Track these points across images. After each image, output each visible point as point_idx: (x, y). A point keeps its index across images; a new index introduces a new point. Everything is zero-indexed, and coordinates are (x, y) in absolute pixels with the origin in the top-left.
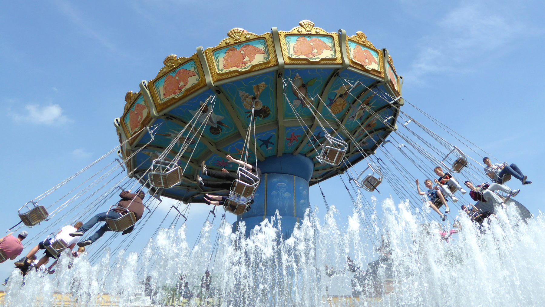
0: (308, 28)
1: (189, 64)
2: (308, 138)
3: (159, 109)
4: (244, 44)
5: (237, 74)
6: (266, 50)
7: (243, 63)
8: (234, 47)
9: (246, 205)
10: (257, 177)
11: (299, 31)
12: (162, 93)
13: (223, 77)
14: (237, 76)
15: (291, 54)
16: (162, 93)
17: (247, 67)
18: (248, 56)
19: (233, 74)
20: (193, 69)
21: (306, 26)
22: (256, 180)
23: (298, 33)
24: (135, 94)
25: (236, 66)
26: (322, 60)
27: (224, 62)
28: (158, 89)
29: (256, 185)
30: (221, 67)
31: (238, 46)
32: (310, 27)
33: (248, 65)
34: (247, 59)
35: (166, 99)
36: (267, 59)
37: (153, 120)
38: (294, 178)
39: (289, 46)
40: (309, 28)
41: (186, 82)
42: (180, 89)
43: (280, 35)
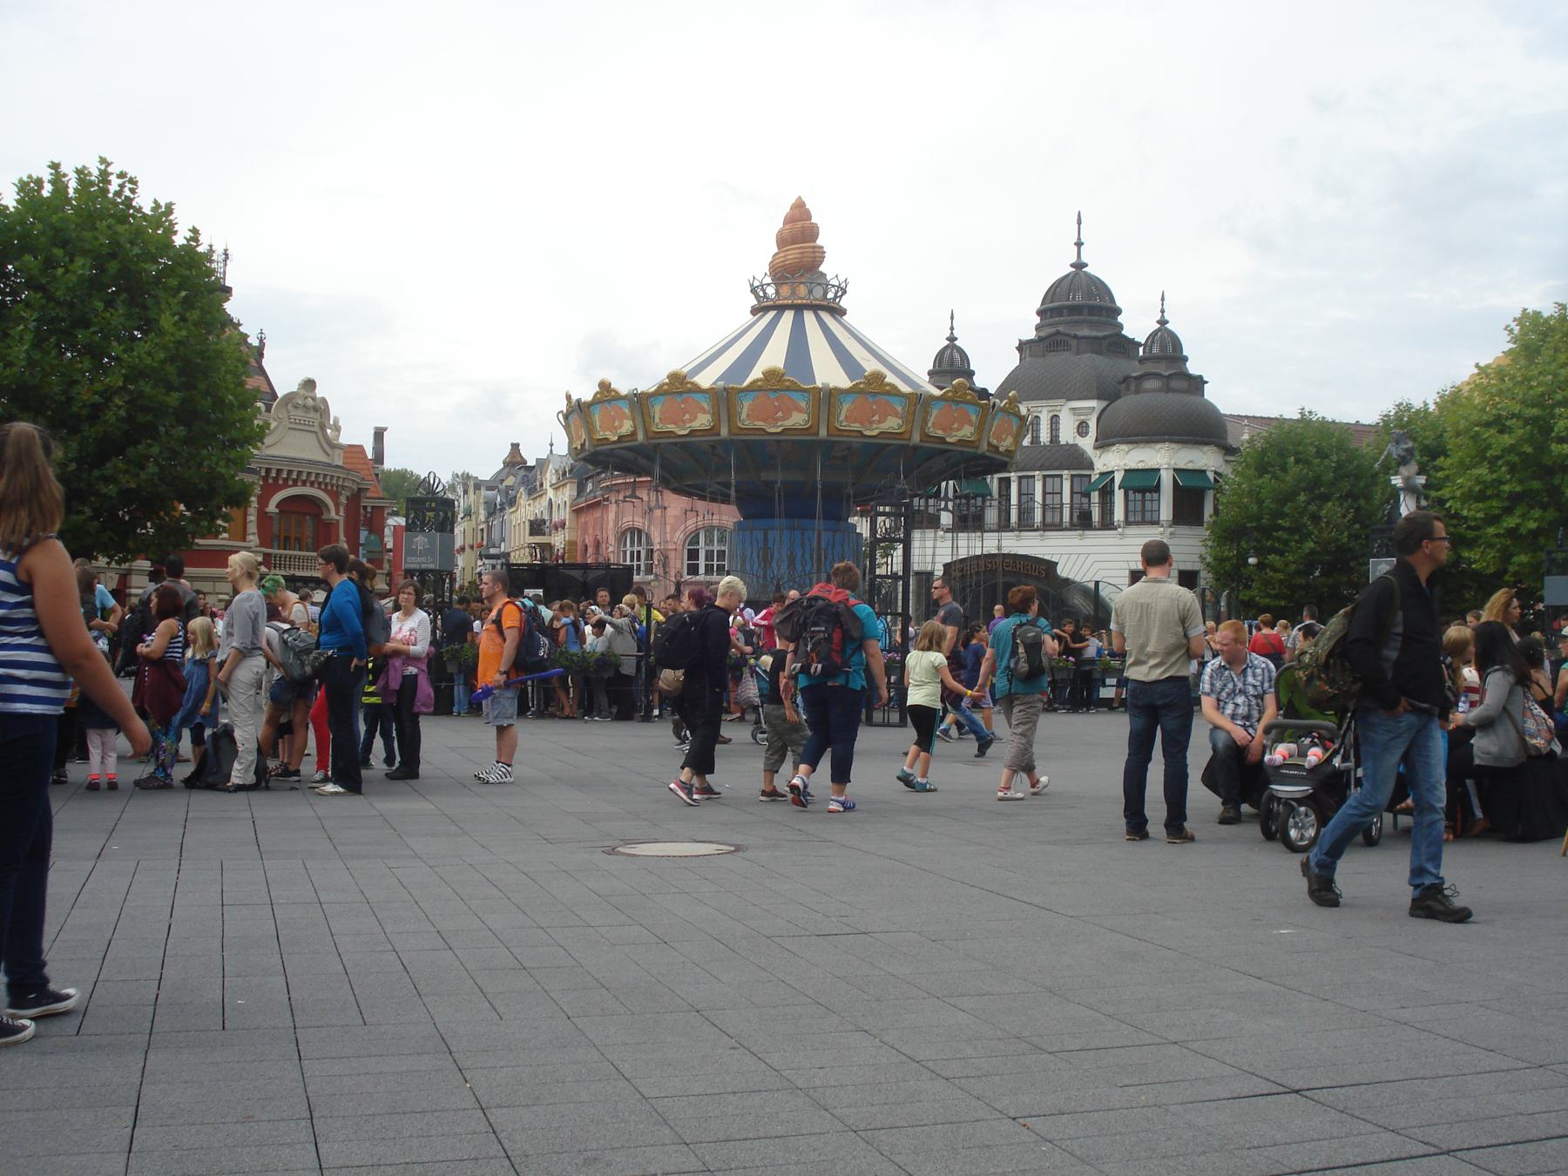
42: (684, 422)
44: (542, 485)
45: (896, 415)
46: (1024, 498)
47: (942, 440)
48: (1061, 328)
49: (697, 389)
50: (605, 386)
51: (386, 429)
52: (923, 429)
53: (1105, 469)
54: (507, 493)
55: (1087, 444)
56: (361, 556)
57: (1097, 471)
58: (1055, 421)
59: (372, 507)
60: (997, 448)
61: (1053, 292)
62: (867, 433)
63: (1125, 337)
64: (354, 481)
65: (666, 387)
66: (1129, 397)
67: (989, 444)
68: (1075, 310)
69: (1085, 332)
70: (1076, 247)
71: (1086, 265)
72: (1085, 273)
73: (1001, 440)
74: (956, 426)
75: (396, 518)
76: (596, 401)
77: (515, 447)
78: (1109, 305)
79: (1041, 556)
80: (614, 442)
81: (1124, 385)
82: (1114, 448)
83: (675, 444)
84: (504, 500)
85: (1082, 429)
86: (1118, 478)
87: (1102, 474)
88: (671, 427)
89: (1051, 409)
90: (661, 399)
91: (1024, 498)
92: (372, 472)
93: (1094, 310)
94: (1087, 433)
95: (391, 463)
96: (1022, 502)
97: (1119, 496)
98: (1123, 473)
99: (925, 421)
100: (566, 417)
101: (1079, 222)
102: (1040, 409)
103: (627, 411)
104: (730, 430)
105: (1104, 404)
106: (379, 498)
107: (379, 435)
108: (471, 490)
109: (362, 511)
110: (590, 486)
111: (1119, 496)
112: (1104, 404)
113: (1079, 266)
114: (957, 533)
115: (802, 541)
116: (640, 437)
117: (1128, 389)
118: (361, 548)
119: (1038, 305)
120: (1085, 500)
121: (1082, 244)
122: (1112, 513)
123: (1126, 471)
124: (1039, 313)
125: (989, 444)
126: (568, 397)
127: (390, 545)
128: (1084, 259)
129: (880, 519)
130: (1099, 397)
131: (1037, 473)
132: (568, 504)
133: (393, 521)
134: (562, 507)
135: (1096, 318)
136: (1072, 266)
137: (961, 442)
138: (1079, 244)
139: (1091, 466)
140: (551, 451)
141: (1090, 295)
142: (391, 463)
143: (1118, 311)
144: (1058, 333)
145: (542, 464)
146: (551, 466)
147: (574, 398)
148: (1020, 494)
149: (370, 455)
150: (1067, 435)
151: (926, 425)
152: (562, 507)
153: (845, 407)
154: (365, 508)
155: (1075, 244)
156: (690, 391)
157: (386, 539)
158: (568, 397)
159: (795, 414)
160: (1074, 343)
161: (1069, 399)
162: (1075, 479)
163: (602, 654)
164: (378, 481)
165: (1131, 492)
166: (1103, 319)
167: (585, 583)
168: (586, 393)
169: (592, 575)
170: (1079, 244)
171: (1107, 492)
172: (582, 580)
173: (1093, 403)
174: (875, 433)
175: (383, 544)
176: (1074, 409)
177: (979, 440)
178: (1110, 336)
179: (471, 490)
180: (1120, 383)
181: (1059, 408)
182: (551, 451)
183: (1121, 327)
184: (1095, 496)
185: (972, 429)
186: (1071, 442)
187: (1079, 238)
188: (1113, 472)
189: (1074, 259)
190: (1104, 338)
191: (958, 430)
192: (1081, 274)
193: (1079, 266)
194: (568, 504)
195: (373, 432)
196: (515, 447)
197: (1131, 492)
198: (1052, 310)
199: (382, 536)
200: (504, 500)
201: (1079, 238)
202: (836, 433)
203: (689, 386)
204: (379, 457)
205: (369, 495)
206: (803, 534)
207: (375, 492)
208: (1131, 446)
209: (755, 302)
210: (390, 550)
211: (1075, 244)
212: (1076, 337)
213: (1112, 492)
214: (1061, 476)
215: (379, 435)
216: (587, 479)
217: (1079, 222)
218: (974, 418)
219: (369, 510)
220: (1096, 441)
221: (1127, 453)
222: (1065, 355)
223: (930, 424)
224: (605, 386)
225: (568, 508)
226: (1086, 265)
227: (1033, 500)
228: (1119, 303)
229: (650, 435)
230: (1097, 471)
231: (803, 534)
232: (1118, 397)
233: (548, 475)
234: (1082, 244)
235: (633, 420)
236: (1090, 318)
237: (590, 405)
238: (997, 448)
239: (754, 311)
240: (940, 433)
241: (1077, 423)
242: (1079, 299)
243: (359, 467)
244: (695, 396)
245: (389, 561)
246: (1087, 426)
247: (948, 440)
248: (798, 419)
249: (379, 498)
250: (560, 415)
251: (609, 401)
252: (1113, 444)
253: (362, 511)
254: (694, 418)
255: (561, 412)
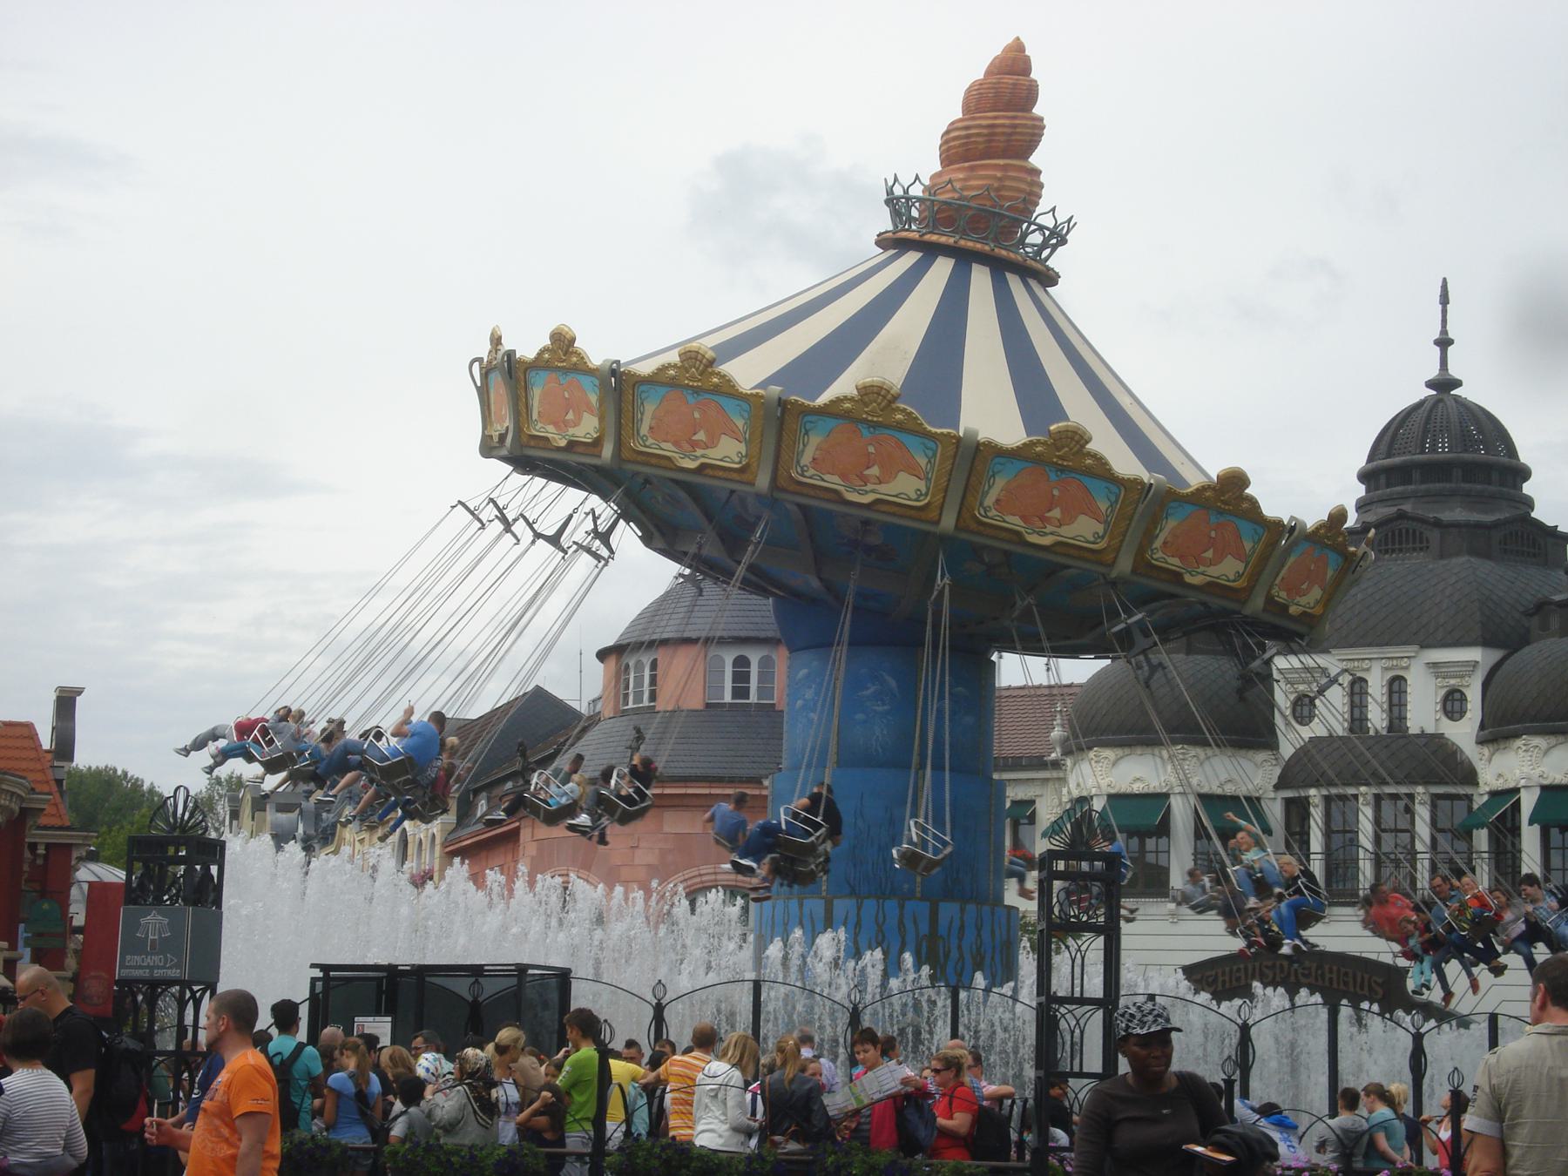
46: (1337, 840)
47: (1177, 577)
48: (1407, 507)
49: (727, 389)
51: (79, 691)
53: (1499, 785)
54: (318, 817)
55: (1463, 733)
56: (21, 943)
57: (1484, 789)
58: (1396, 687)
59: (48, 846)
60: (1284, 608)
61: (1392, 437)
62: (1033, 539)
63: (1539, 525)
64: (13, 794)
66: (1548, 642)
67: (1270, 600)
68: (1436, 470)
69: (1456, 514)
70: (1437, 350)
71: (1458, 384)
72: (1457, 399)
73: (1294, 589)
74: (1209, 554)
75: (94, 867)
76: (539, 364)
78: (1506, 460)
79: (1373, 957)
81: (1535, 620)
82: (1519, 742)
83: (676, 482)
84: (312, 832)
85: (1453, 704)
86: (1528, 802)
87: (1495, 794)
88: (668, 449)
89: (1389, 663)
91: (1337, 840)
92: (50, 775)
93: (1473, 471)
94: (1462, 713)
95: (86, 757)
96: (1334, 847)
97: (1530, 838)
98: (1537, 792)
99: (1149, 536)
100: (485, 374)
101: (1444, 300)
102: (1365, 665)
103: (593, 398)
104: (774, 478)
105: (1495, 655)
106: (61, 828)
107: (66, 703)
108: (246, 811)
109: (27, 854)
110: (482, 806)
111: (1530, 838)
112: (1495, 655)
113: (1444, 384)
115: (901, 923)
117: (1545, 627)
118: (22, 927)
119: (1360, 460)
120: (1461, 845)
121: (1451, 342)
122: (1516, 853)
123: (1544, 788)
124: (1364, 477)
125: (1270, 600)
126: (496, 341)
127: (79, 920)
128: (1454, 371)
130: (1486, 642)
132: (438, 841)
133: (87, 873)
134: (426, 845)
135: (1479, 487)
136: (1430, 384)
137: (1213, 587)
138: (1444, 343)
139: (1470, 777)
141: (1465, 441)
142: (86, 757)
143: (1524, 473)
144: (1402, 516)
147: (507, 345)
148: (1328, 833)
149: (46, 740)
150: (1423, 714)
151: (1151, 543)
152: (426, 845)
154: (33, 847)
155: (1437, 343)
156: (716, 390)
157: (73, 909)
158: (496, 341)
159: (902, 476)
160: (1434, 535)
161: (1425, 645)
162: (1440, 803)
163: (511, 1152)
164: (62, 793)
165: (1554, 832)
166: (1492, 488)
167: (475, 1006)
168: (528, 344)
169: (490, 988)
170: (1444, 343)
171: (1506, 829)
172: (470, 999)
173: (1474, 654)
174: (1047, 541)
175: (65, 917)
176: (1435, 665)
177: (1249, 590)
178: (1506, 522)
179: (246, 811)
180: (1528, 614)
181: (1404, 663)
183: (1529, 503)
184: (1481, 838)
185: (1240, 567)
186: (1430, 730)
187: (1444, 331)
188: (1516, 790)
189: (1433, 372)
190: (1495, 525)
191: (1212, 563)
192: (1450, 403)
193: (1444, 384)
194: (438, 841)
195: (54, 697)
197: (1554, 832)
198: (1389, 471)
199: (64, 903)
200: (312, 832)
201: (1444, 331)
204: (65, 744)
205: (43, 821)
206: (902, 907)
207: (56, 812)
208: (1552, 740)
210: (79, 930)
211: (1437, 343)
212: (1438, 524)
213: (1516, 831)
214: (1411, 797)
215: (66, 703)
216: (476, 792)
217: (1444, 300)
219: (41, 851)
220: (1482, 727)
221: (1546, 753)
222: (1416, 560)
223: (1158, 543)
225: (438, 848)
226: (1458, 384)
227: (1354, 843)
228: (1525, 457)
230: (1484, 789)
231: (902, 907)
232: (1524, 641)
234: (1451, 342)
235: (601, 419)
236: (1467, 486)
238: (1285, 608)
240: (1174, 563)
241: (1443, 692)
242: (1444, 450)
243: (24, 765)
244: (722, 400)
245: (76, 951)
246: (1463, 699)
247: (1188, 579)
248: (905, 487)
249: (61, 828)
250: (476, 366)
252: (1517, 735)
253: (27, 854)
254: (712, 443)
255: (480, 360)
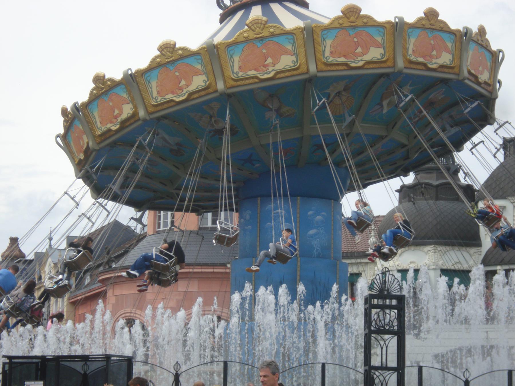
0: (257, 29)
1: (194, 58)
2: (416, 103)
3: (98, 140)
4: (267, 40)
5: (256, 80)
6: (294, 51)
7: (265, 66)
8: (254, 42)
9: (170, 279)
10: (172, 254)
11: (364, 23)
12: (98, 120)
13: (239, 83)
14: (256, 83)
15: (327, 57)
16: (98, 120)
17: (270, 72)
18: (271, 57)
19: (243, 81)
20: (379, 39)
21: (255, 26)
22: (171, 257)
23: (363, 24)
24: (111, 80)
25: (256, 70)
26: (368, 63)
27: (240, 63)
28: (93, 114)
29: (171, 263)
30: (236, 69)
31: (260, 41)
32: (260, 27)
33: (270, 69)
34: (269, 60)
35: (103, 128)
36: (295, 62)
37: (94, 153)
38: (299, 201)
39: (233, 61)
40: (260, 28)
41: (366, 51)
42: (181, 89)
43: (314, 30)
44: (40, 278)
45: (377, 45)
50: (99, 80)
52: (404, 56)
65: (158, 60)
77: (14, 241)
80: (117, 131)
90: (156, 72)
104: (225, 82)
110: (88, 280)
114: (470, 139)
116: (142, 113)
129: (374, 311)
131: (499, 267)
140: (50, 245)
145: (41, 258)
146: (50, 260)
151: (407, 52)
153: (329, 42)
156: (182, 57)
182: (50, 245)
196: (14, 241)
202: (325, 68)
203: (180, 52)
209: (221, 11)
218: (449, 45)
223: (410, 52)
224: (99, 80)
229: (151, 110)
233: (47, 269)
237: (87, 105)
239: (223, 18)
251: (105, 93)
